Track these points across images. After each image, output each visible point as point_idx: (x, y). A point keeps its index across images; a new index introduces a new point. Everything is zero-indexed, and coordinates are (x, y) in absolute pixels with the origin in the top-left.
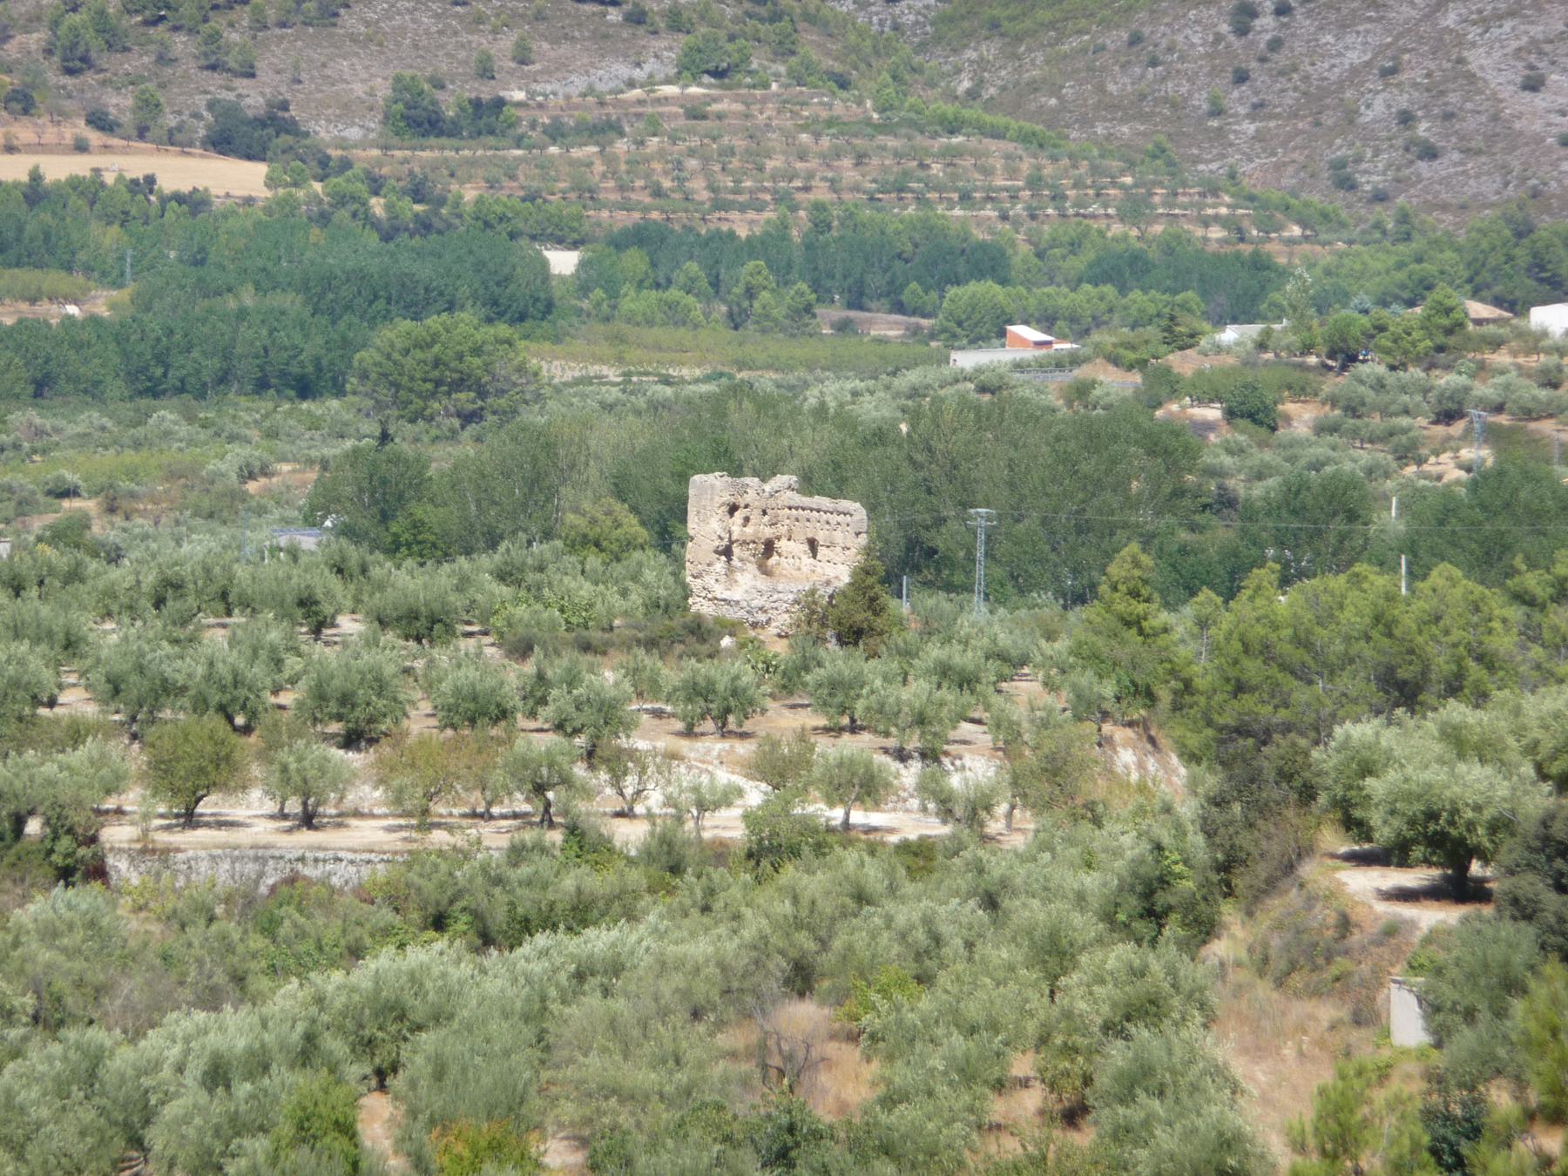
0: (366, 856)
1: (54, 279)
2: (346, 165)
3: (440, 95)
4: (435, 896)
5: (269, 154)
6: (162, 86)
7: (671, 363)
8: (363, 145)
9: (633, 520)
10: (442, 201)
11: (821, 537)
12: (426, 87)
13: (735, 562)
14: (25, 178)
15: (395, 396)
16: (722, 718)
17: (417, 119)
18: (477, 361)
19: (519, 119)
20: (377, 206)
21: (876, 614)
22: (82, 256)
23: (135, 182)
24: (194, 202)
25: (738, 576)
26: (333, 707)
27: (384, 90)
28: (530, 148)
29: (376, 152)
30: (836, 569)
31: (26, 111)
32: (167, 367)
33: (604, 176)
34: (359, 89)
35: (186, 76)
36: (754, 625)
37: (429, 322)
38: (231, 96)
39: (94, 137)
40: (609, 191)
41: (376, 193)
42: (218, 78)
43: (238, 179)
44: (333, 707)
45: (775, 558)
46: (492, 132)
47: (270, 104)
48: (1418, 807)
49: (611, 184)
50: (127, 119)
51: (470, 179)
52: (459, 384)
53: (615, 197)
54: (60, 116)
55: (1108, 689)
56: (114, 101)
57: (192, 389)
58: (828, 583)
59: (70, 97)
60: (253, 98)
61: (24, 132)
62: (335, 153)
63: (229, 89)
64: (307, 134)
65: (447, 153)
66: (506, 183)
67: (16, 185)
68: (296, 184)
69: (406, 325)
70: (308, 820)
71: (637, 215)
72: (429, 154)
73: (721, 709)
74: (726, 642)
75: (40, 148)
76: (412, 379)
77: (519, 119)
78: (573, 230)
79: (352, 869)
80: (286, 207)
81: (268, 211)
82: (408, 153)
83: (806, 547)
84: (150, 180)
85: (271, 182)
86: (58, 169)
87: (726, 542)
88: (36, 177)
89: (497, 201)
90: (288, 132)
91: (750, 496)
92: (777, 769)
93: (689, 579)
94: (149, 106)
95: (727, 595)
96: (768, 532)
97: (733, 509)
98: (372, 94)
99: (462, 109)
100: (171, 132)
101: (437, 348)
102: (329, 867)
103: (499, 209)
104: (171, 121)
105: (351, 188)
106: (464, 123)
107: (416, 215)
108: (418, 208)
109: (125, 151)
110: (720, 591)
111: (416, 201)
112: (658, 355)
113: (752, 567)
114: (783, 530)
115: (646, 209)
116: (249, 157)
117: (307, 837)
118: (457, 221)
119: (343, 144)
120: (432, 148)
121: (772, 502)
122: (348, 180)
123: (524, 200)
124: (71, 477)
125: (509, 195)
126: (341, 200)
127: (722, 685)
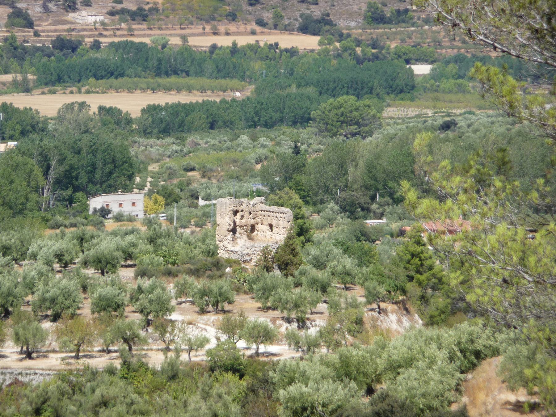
0: (48, 372)
1: (235, 82)
2: (349, 36)
3: (385, 9)
4: (36, 400)
5: (321, 33)
6: (284, 9)
7: (454, 108)
8: (356, 28)
9: (297, 196)
10: (383, 48)
11: (274, 223)
12: (380, 6)
13: (237, 235)
14: (231, 45)
15: (326, 128)
16: (216, 304)
17: (376, 18)
18: (357, 114)
19: (414, 17)
20: (359, 50)
21: (294, 256)
22: (248, 73)
23: (271, 45)
24: (292, 52)
25: (238, 241)
26: (48, 304)
27: (364, 7)
28: (417, 27)
29: (360, 31)
30: (279, 236)
31: (234, 20)
32: (260, 117)
33: (444, 37)
34: (355, 8)
35: (293, 5)
36: (244, 262)
37: (339, 99)
38: (309, 12)
39: (258, 29)
40: (446, 42)
41: (359, 46)
42: (304, 5)
43: (309, 43)
44: (48, 304)
45: (256, 232)
46: (404, 21)
47: (323, 15)
48: (298, 405)
49: (447, 39)
50: (271, 22)
51: (394, 39)
52: (350, 123)
53: (448, 44)
54: (246, 21)
55: (382, 290)
56: (267, 15)
57: (269, 125)
58: (276, 243)
59: (250, 14)
60: (316, 12)
61: (232, 28)
62: (345, 32)
63: (308, 9)
64: (336, 25)
65: (386, 30)
66: (408, 40)
67: (228, 47)
68: (329, 44)
69: (331, 100)
70: (29, 355)
71: (456, 51)
72: (379, 31)
73: (213, 302)
74: (228, 270)
75: (238, 33)
76: (333, 121)
77: (414, 17)
78: (431, 57)
79: (42, 378)
80: (326, 52)
81: (319, 54)
82: (372, 30)
83: (268, 227)
84: (277, 44)
85: (320, 43)
86: (243, 41)
87: (232, 226)
88: (235, 44)
89: (403, 47)
90: (328, 24)
91: (244, 207)
92: (229, 328)
93: (218, 242)
94: (278, 17)
95: (233, 249)
96: (252, 222)
97: (235, 213)
98: (360, 9)
99: (393, 13)
100: (286, 26)
101: (342, 109)
102: (32, 377)
103: (403, 50)
104: (287, 22)
105: (349, 44)
106: (393, 19)
107: (373, 54)
108: (374, 51)
109: (269, 34)
110: (230, 247)
111: (373, 48)
112: (450, 104)
113: (245, 237)
114: (259, 220)
115: (459, 48)
116: (314, 34)
117: (28, 363)
118: (388, 55)
119: (348, 28)
120: (381, 28)
121: (253, 209)
122: (348, 42)
123: (413, 46)
124: (193, 164)
125: (407, 46)
126: (345, 49)
127: (215, 290)
